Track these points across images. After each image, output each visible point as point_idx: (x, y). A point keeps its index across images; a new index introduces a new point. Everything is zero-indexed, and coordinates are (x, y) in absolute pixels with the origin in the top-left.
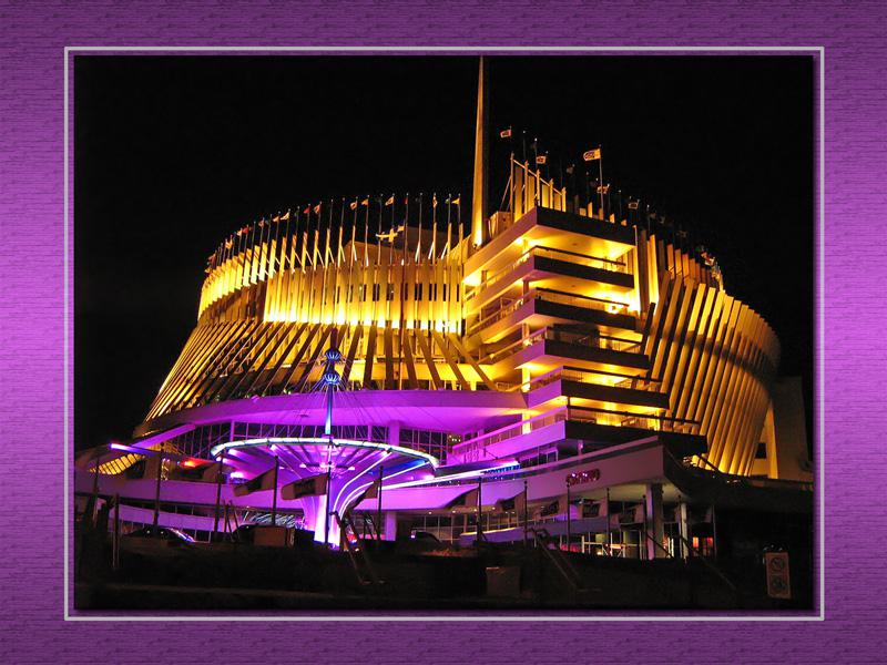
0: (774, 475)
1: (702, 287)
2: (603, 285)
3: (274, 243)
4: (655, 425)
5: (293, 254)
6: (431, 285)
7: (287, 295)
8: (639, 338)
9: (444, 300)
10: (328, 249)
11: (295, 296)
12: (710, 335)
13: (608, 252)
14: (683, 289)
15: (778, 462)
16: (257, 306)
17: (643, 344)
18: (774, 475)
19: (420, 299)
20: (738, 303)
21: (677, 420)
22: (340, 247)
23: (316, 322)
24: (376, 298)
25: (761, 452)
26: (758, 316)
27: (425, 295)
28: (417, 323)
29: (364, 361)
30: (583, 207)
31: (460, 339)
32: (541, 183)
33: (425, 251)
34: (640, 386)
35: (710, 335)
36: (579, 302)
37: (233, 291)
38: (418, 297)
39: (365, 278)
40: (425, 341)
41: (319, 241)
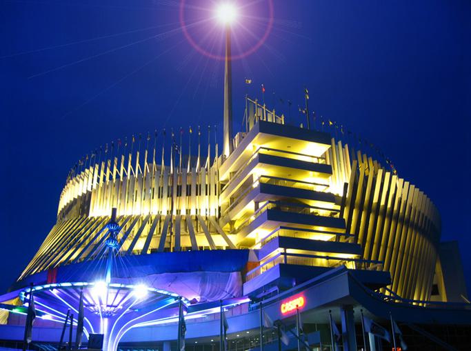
0: (444, 299)
1: (380, 172)
2: (311, 173)
3: (97, 166)
4: (351, 266)
5: (122, 168)
6: (197, 185)
7: (104, 198)
8: (338, 208)
9: (206, 194)
10: (138, 165)
11: (139, 193)
12: (389, 205)
13: (311, 150)
14: (366, 178)
15: (446, 288)
16: (86, 208)
17: (342, 212)
18: (444, 299)
19: (190, 195)
20: (407, 183)
21: (372, 262)
22: (146, 163)
23: (137, 214)
24: (160, 196)
25: (435, 291)
26: (422, 193)
27: (193, 192)
28: (188, 211)
29: (145, 239)
30: (92, 166)
31: (217, 220)
32: (267, 112)
33: (193, 165)
34: (342, 240)
35: (389, 205)
36: (298, 185)
37: (72, 200)
38: (189, 194)
39: (154, 184)
40: (193, 224)
41: (125, 162)
